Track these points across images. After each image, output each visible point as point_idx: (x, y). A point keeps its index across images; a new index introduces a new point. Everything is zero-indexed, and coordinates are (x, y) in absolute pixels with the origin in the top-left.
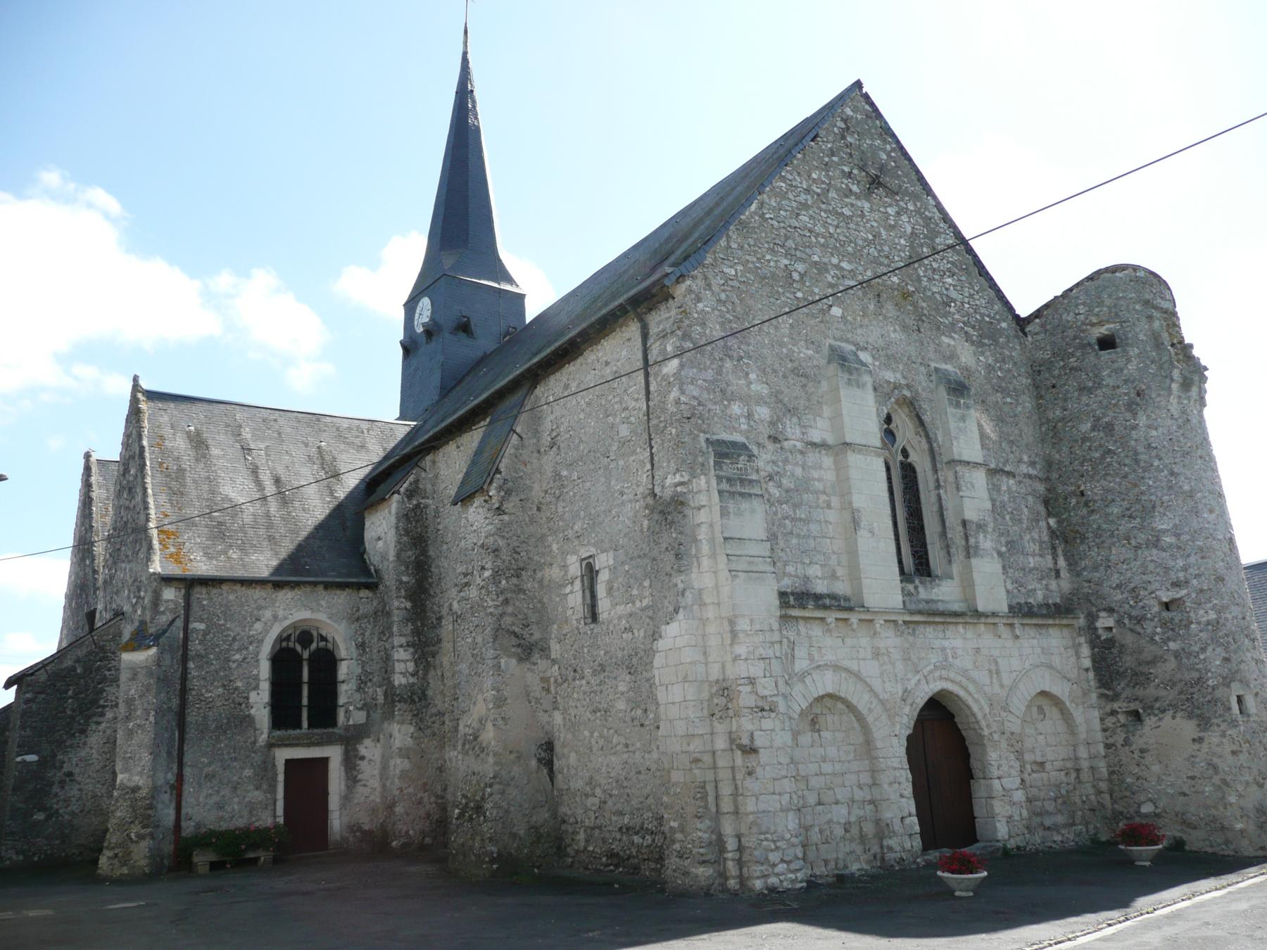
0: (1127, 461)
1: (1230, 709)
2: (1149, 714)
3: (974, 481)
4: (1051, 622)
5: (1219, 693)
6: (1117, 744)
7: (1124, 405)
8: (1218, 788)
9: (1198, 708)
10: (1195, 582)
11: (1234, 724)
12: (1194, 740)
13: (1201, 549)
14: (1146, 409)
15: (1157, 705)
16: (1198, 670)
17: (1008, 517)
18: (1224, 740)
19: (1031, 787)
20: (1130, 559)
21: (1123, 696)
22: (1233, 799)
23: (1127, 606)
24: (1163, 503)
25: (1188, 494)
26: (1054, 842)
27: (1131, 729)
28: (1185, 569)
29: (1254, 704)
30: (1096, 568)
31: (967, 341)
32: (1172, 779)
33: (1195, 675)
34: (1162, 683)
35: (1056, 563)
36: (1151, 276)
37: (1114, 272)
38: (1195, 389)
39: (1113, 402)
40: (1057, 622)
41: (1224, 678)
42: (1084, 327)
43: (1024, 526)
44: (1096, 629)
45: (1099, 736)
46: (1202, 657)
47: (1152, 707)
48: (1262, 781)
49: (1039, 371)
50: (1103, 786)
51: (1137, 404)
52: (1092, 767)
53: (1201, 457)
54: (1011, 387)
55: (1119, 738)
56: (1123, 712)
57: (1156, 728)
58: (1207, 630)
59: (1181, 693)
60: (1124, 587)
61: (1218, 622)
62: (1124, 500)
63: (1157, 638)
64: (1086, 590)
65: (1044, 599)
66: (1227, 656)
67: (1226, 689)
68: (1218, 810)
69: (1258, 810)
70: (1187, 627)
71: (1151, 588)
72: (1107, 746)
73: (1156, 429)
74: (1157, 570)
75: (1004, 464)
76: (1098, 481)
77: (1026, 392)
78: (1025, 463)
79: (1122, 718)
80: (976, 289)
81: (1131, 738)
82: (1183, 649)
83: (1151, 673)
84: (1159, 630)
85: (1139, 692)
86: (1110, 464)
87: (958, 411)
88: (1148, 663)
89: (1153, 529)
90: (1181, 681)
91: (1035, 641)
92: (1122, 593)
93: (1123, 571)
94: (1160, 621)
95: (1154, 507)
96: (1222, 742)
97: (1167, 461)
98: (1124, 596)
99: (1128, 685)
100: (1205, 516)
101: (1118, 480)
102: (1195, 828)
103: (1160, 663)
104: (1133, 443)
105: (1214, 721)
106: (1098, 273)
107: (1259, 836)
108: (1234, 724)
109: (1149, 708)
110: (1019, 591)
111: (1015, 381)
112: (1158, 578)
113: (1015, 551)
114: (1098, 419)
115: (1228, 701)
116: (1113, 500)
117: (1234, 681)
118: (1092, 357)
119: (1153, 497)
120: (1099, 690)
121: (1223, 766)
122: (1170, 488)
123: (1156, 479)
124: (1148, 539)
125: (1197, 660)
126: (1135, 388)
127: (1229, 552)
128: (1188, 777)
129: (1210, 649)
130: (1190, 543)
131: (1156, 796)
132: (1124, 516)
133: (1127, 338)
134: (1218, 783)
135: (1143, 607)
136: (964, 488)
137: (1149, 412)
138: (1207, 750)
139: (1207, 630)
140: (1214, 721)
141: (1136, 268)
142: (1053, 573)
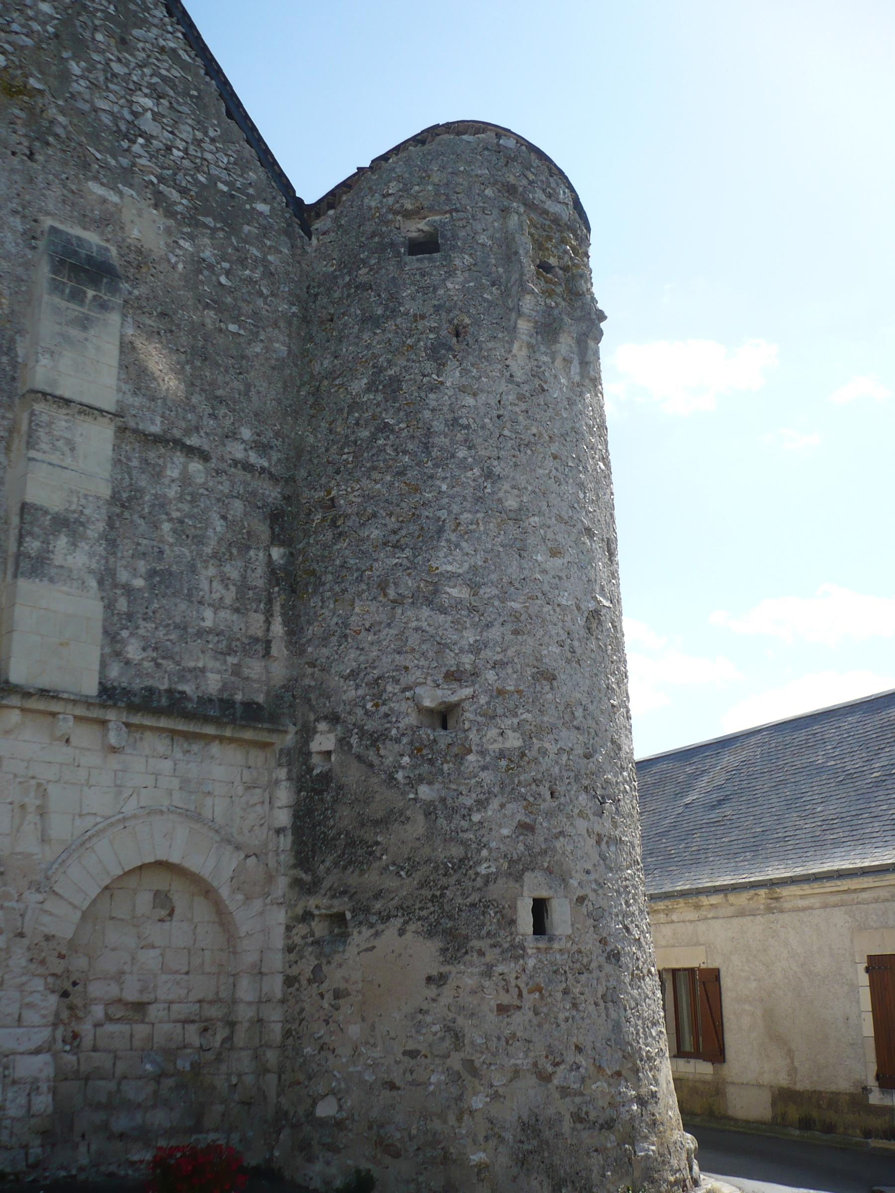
0: (410, 447)
1: (512, 922)
2: (360, 923)
3: (78, 439)
4: (210, 730)
5: (496, 890)
6: (301, 977)
7: (426, 348)
8: (456, 1078)
9: (451, 917)
10: (491, 675)
11: (516, 952)
12: (429, 979)
13: (516, 616)
14: (463, 358)
15: (378, 905)
16: (463, 843)
17: (166, 527)
18: (487, 984)
19: (95, 1049)
20: (381, 623)
21: (326, 884)
22: (478, 1102)
23: (360, 712)
24: (459, 524)
25: (512, 515)
26: (132, 1164)
27: (327, 949)
28: (476, 649)
29: (568, 917)
30: (325, 640)
31: (156, 206)
32: (377, 1053)
33: (457, 851)
34: (394, 864)
35: (268, 630)
36: (533, 156)
37: (459, 134)
38: (565, 343)
39: (409, 341)
40: (228, 733)
41: (512, 862)
42: (390, 216)
43: (208, 550)
44: (309, 754)
45: (276, 961)
46: (476, 817)
47: (367, 910)
48: (550, 1069)
49: (316, 295)
50: (272, 1057)
51: (450, 349)
52: (260, 1020)
53: (555, 457)
54: (246, 308)
55: (306, 967)
56: (320, 915)
57: (368, 950)
58: (496, 768)
59: (421, 886)
60: (362, 674)
61: (523, 755)
62: (390, 515)
63: (400, 776)
64: (307, 681)
65: (221, 690)
66: (528, 820)
67: (511, 884)
68: (445, 1122)
69: (524, 1126)
70: (460, 758)
71: (406, 680)
72: (290, 981)
73: (475, 395)
74: (424, 647)
75: (188, 432)
76: (358, 481)
77: (282, 324)
78: (243, 442)
79: (320, 928)
80: (211, 133)
81: (325, 968)
82: (443, 800)
83: (377, 843)
84: (406, 760)
85: (352, 879)
86: (382, 450)
87: (71, 306)
88: (376, 823)
89: (430, 570)
90: (428, 861)
91: (167, 765)
92: (358, 687)
93: (366, 645)
94: (411, 743)
95: (440, 531)
96: (483, 987)
97: (482, 453)
98: (360, 692)
99: (336, 864)
100: (539, 558)
101: (388, 478)
102: (397, 1155)
103: (396, 825)
104: (427, 414)
105: (476, 943)
106: (433, 132)
107: (515, 1179)
108: (516, 952)
109: (362, 910)
110: (158, 665)
111: (260, 302)
112: (422, 662)
113: (169, 591)
114: (381, 370)
115: (513, 907)
116: (374, 515)
117: (533, 870)
118: (391, 268)
119: (443, 514)
120: (293, 872)
121: (474, 1035)
122: (478, 500)
123: (455, 482)
124: (418, 587)
125: (465, 824)
126: (450, 322)
127: (583, 633)
128: (405, 1053)
129: (495, 804)
130: (496, 603)
131: (343, 1085)
132: (385, 544)
133: (455, 237)
134: (457, 1066)
135: (387, 715)
136: (44, 446)
137: (466, 364)
138: (450, 1000)
139: (496, 768)
140: (476, 943)
141: (501, 132)
142: (259, 647)
